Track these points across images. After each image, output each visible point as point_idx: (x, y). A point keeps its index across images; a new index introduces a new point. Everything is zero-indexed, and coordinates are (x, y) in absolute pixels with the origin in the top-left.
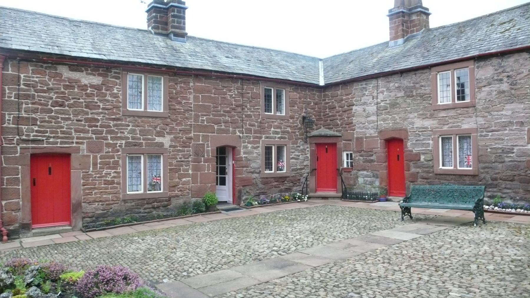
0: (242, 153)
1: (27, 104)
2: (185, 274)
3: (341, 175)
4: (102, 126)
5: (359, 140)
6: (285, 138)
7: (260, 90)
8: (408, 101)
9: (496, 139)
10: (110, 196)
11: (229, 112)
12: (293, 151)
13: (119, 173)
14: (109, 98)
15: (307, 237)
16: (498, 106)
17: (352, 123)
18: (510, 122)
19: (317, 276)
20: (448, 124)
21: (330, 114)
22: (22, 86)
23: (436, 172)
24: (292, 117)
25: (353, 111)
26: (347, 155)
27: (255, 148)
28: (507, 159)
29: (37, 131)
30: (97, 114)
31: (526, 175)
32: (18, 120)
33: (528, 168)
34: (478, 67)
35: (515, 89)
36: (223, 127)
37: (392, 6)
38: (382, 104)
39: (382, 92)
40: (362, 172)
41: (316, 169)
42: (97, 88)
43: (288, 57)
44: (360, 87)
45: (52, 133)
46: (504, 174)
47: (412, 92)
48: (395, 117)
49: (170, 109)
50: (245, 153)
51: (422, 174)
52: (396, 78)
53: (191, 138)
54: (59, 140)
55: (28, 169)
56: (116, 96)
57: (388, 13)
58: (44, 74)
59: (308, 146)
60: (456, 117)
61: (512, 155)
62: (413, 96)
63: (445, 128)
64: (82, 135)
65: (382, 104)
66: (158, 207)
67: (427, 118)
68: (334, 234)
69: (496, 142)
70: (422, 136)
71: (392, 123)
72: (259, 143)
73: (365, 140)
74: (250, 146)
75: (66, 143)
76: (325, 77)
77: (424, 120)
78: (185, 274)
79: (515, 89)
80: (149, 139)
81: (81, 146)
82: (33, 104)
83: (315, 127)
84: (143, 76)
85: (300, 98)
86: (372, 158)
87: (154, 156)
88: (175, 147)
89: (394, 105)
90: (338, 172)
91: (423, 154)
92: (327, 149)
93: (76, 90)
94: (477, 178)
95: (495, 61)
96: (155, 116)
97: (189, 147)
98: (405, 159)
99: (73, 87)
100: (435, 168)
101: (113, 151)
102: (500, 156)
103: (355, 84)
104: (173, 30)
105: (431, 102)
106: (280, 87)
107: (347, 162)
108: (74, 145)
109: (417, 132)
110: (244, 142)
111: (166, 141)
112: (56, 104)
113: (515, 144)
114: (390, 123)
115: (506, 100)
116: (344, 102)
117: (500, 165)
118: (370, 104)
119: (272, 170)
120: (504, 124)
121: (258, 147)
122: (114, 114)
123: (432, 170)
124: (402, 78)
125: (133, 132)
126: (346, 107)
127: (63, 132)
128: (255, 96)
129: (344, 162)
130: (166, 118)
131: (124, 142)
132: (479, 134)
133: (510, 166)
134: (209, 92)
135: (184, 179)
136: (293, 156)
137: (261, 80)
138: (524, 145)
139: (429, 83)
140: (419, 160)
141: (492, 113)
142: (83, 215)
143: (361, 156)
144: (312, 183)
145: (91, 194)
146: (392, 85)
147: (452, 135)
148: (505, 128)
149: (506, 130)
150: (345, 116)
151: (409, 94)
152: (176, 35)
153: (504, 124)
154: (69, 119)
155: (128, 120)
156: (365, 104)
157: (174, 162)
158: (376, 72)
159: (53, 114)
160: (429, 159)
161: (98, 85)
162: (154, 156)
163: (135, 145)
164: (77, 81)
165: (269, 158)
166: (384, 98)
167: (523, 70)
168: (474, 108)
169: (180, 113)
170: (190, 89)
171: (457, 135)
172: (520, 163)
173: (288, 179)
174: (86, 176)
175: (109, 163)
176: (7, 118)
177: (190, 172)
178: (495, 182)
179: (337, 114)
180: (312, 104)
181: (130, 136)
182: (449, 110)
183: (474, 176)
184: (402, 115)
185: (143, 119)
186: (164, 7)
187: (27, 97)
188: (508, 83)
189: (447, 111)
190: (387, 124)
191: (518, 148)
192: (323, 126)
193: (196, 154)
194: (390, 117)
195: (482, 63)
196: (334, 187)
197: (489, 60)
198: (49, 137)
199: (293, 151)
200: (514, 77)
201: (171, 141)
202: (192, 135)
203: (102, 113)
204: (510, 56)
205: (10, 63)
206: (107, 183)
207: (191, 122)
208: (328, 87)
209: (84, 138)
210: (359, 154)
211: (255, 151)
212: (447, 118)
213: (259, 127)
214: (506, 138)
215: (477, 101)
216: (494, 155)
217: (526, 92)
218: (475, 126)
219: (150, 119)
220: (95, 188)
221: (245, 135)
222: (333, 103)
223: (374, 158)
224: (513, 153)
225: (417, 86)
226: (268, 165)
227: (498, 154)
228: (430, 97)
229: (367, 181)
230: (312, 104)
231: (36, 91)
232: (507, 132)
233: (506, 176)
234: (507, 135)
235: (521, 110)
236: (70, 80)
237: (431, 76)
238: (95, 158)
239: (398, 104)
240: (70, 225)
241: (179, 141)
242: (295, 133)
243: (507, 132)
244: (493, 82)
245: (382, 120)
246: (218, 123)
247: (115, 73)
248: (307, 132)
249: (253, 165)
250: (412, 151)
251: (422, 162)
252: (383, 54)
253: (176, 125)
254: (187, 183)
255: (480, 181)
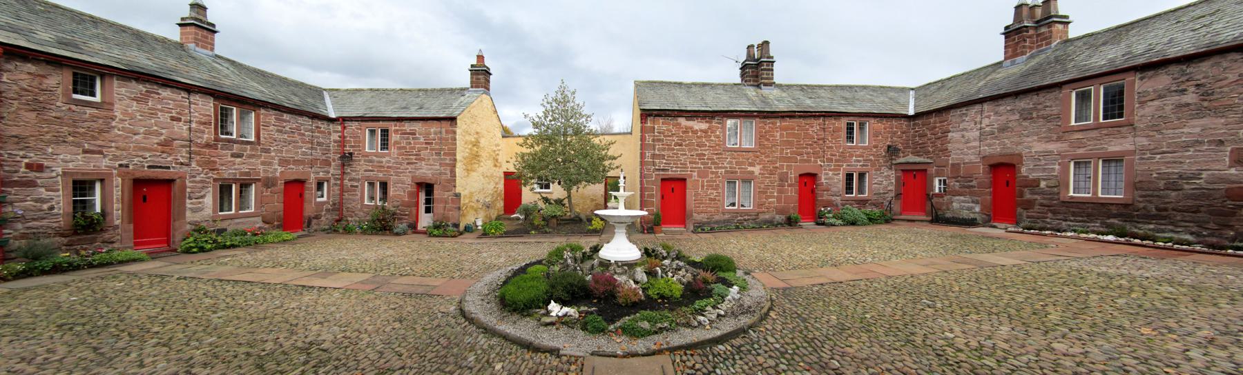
0: (823, 179)
1: (659, 145)
2: (771, 269)
3: (930, 199)
4: (708, 159)
5: (955, 167)
6: (867, 166)
7: (843, 122)
8: (1025, 124)
9: (1168, 162)
10: (713, 209)
11: (810, 145)
12: (876, 177)
13: (719, 193)
14: (713, 138)
15: (885, 252)
16: (1175, 122)
17: (947, 149)
18: (1197, 141)
19: (890, 282)
20: (1085, 147)
21: (921, 142)
22: (656, 134)
23: (1062, 199)
24: (876, 147)
25: (949, 138)
26: (940, 181)
27: (835, 175)
28: (1186, 187)
29: (665, 163)
30: (705, 150)
31: (1223, 207)
32: (654, 156)
33: (1227, 197)
34: (1141, 79)
35: (1210, 101)
36: (805, 158)
37: (1010, 21)
38: (987, 129)
39: (989, 117)
40: (957, 198)
41: (901, 194)
42: (705, 131)
43: (874, 91)
44: (959, 113)
45: (674, 164)
46: (1180, 204)
47: (1031, 114)
48: (1004, 142)
49: (760, 145)
50: (825, 179)
51: (1042, 201)
52: (1009, 100)
53: (777, 168)
54: (679, 169)
55: (659, 189)
56: (718, 137)
57: (1003, 31)
58: (669, 124)
59: (893, 172)
60: (1098, 138)
61: (1198, 182)
62: (1032, 118)
63: (1081, 151)
64: (694, 166)
65: (987, 129)
66: (748, 220)
67: (1053, 141)
68: (917, 252)
69: (1169, 166)
70: (1043, 161)
71: (1001, 148)
72: (840, 170)
73: (962, 165)
74: (831, 173)
75: (683, 171)
76: (915, 106)
77: (1047, 144)
78: (771, 269)
79: (1210, 101)
80: (742, 168)
81: (693, 173)
82: (663, 145)
83: (902, 155)
84: (739, 121)
85: (885, 129)
86: (971, 184)
87: (747, 181)
88: (763, 174)
89: (1003, 129)
90: (928, 197)
91: (1044, 180)
92: (915, 175)
93: (690, 134)
94: (1131, 207)
95: (1174, 69)
96: (748, 151)
97: (775, 174)
98: (1017, 185)
99: (688, 132)
100: (1061, 195)
101: (715, 177)
102: (1175, 182)
103: (952, 111)
104: (763, 81)
105: (1059, 124)
106: (863, 119)
107: (940, 188)
108: (689, 172)
109: (1036, 157)
110: (825, 170)
111: (756, 170)
112: (677, 144)
113: (1204, 168)
114: (997, 148)
115: (1190, 115)
116: (937, 129)
117: (1174, 194)
118: (971, 129)
119: (852, 194)
120: (1185, 144)
121: (839, 174)
122: (717, 150)
123: (1056, 197)
124: (1017, 100)
125: (730, 163)
126: (940, 134)
127: (681, 164)
128: (837, 130)
129: (935, 187)
130: (757, 152)
131: (723, 170)
132: (1137, 157)
133: (1192, 194)
134: (793, 129)
135: (770, 200)
136: (876, 182)
137: (843, 116)
138: (1222, 168)
139: (1057, 102)
140: (1038, 186)
141: (1164, 131)
142: (694, 222)
143: (957, 181)
144: (897, 207)
145: (699, 207)
146: (1002, 108)
147: (1091, 158)
148: (1186, 149)
149: (1190, 151)
150: (938, 143)
151: (1026, 116)
152: (766, 85)
153: (1185, 144)
154: (685, 154)
155: (727, 154)
156: (965, 130)
157: (762, 186)
158: (981, 96)
159: (675, 151)
160: (1053, 185)
161: (706, 130)
162: (747, 181)
163: (732, 173)
164: (691, 128)
165: (850, 183)
166: (990, 122)
167: (1227, 75)
168: (1131, 127)
169: (768, 148)
170: (777, 128)
171: (1099, 158)
172: (1212, 192)
173: (870, 202)
174: (697, 195)
175: (712, 186)
176: (647, 154)
177: (775, 194)
178: (1164, 213)
179: (929, 142)
180: (899, 133)
181: (728, 166)
182: (1088, 132)
183: (1126, 206)
184: (1016, 139)
185: (739, 153)
186: (755, 63)
187: (659, 140)
188: (1197, 93)
189: (1085, 132)
190: (993, 149)
191: (1210, 172)
192: (912, 153)
193: (781, 180)
194: (998, 142)
195: (1150, 73)
196: (923, 210)
197: (1163, 68)
198: (672, 167)
199: (876, 177)
200: (1210, 86)
201: (761, 170)
202: (778, 165)
203: (708, 150)
204: (1205, 60)
205: (649, 118)
206: (711, 200)
207: (776, 155)
208: (918, 116)
209: (695, 168)
210: (954, 179)
211: (836, 177)
212: (1085, 140)
213: (839, 156)
214: (1188, 161)
215: (1136, 118)
216: (1165, 181)
217: (1232, 103)
218: (1132, 148)
219: (744, 153)
220: (702, 203)
221: (826, 164)
222: (924, 130)
223: (974, 183)
224: (1201, 178)
225: (1039, 107)
226: (849, 189)
227: (1171, 181)
228: (1058, 118)
229: (964, 206)
230: (899, 133)
231: (664, 136)
232: (1190, 153)
233: (1184, 206)
234: (1189, 157)
235: (1220, 126)
236: (687, 128)
237: (1061, 95)
238: (703, 182)
239: (1009, 128)
240: (685, 228)
241: (767, 170)
242: (878, 160)
243: (1190, 153)
244: (1168, 94)
245: (986, 146)
246: (801, 154)
247: (718, 120)
248: (892, 159)
249: (835, 189)
250: (1028, 177)
251: (1043, 189)
252: (994, 76)
253: (765, 157)
254: (773, 202)
255: (1137, 211)
